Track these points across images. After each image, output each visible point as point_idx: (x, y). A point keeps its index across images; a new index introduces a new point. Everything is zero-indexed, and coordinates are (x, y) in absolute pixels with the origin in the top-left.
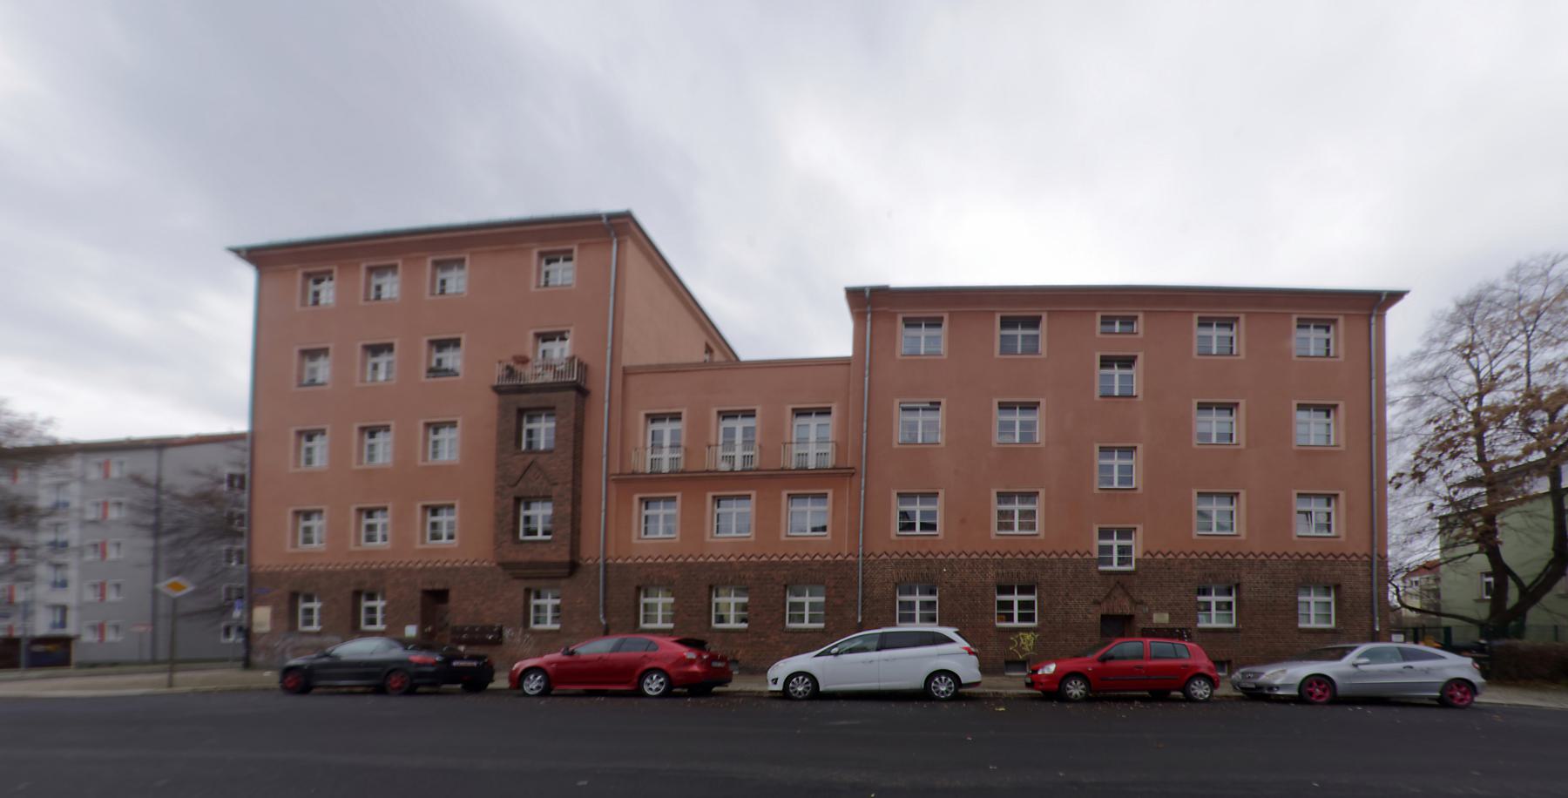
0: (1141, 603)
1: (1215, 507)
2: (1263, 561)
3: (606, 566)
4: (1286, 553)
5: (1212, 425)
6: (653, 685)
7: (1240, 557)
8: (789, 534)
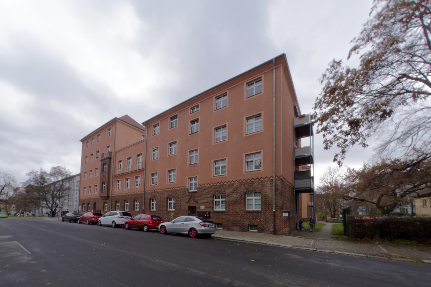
0: (198, 202)
1: (254, 159)
2: (233, 184)
3: (112, 196)
4: (240, 180)
5: (221, 134)
6: (145, 228)
7: (225, 183)
8: (247, 171)
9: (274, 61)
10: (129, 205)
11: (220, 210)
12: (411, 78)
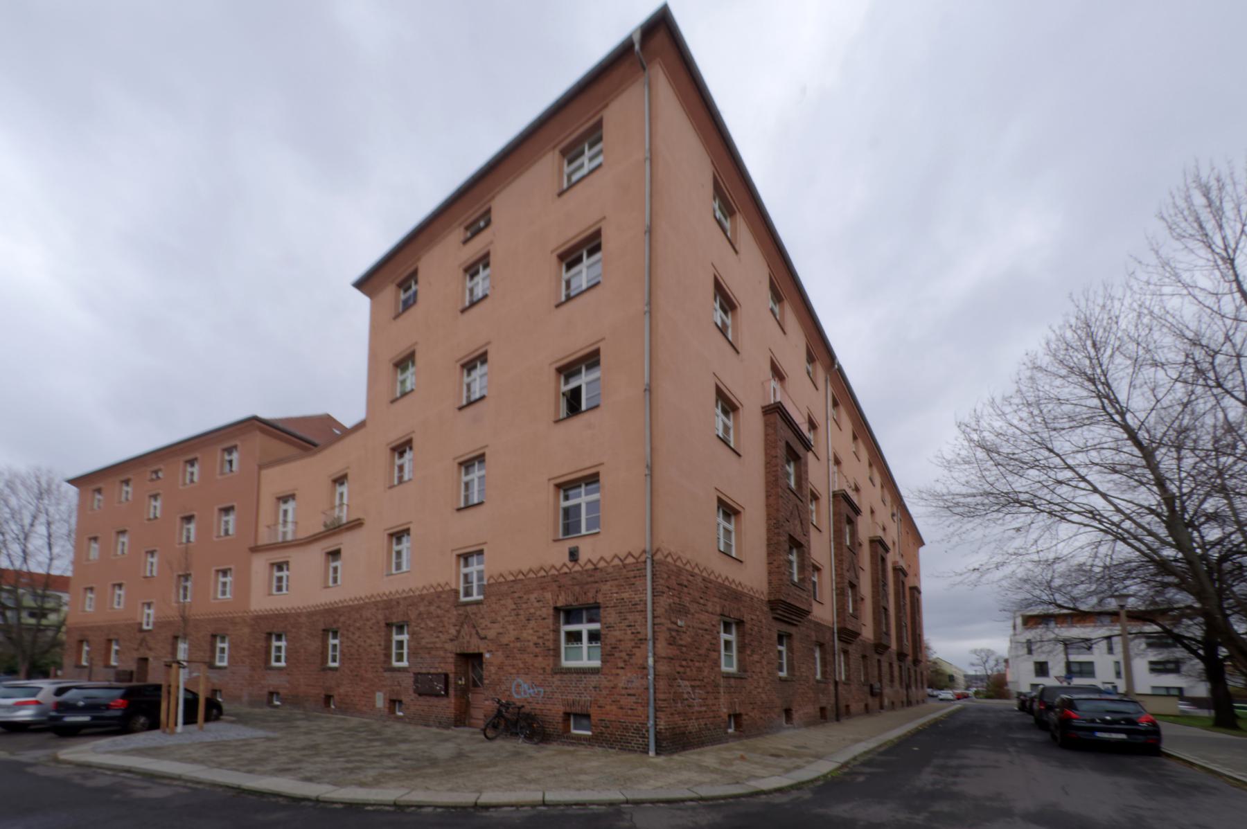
9: (637, 47)
10: (287, 649)
11: (585, 663)
12: (1197, 255)
